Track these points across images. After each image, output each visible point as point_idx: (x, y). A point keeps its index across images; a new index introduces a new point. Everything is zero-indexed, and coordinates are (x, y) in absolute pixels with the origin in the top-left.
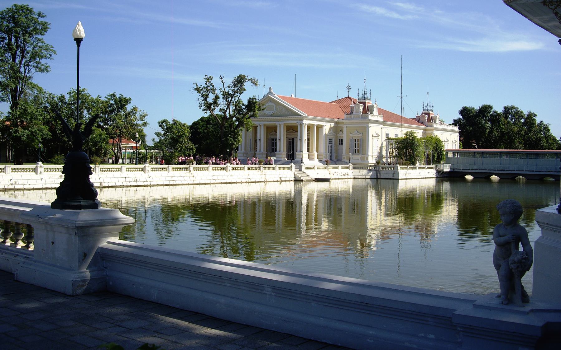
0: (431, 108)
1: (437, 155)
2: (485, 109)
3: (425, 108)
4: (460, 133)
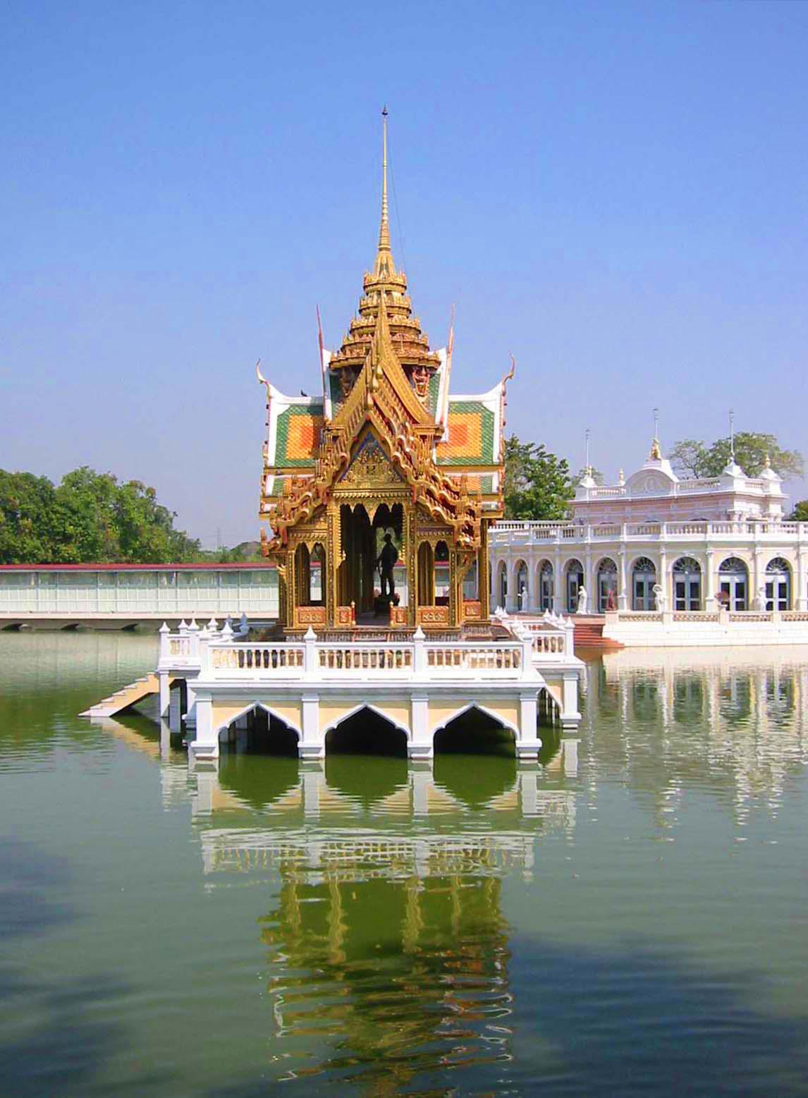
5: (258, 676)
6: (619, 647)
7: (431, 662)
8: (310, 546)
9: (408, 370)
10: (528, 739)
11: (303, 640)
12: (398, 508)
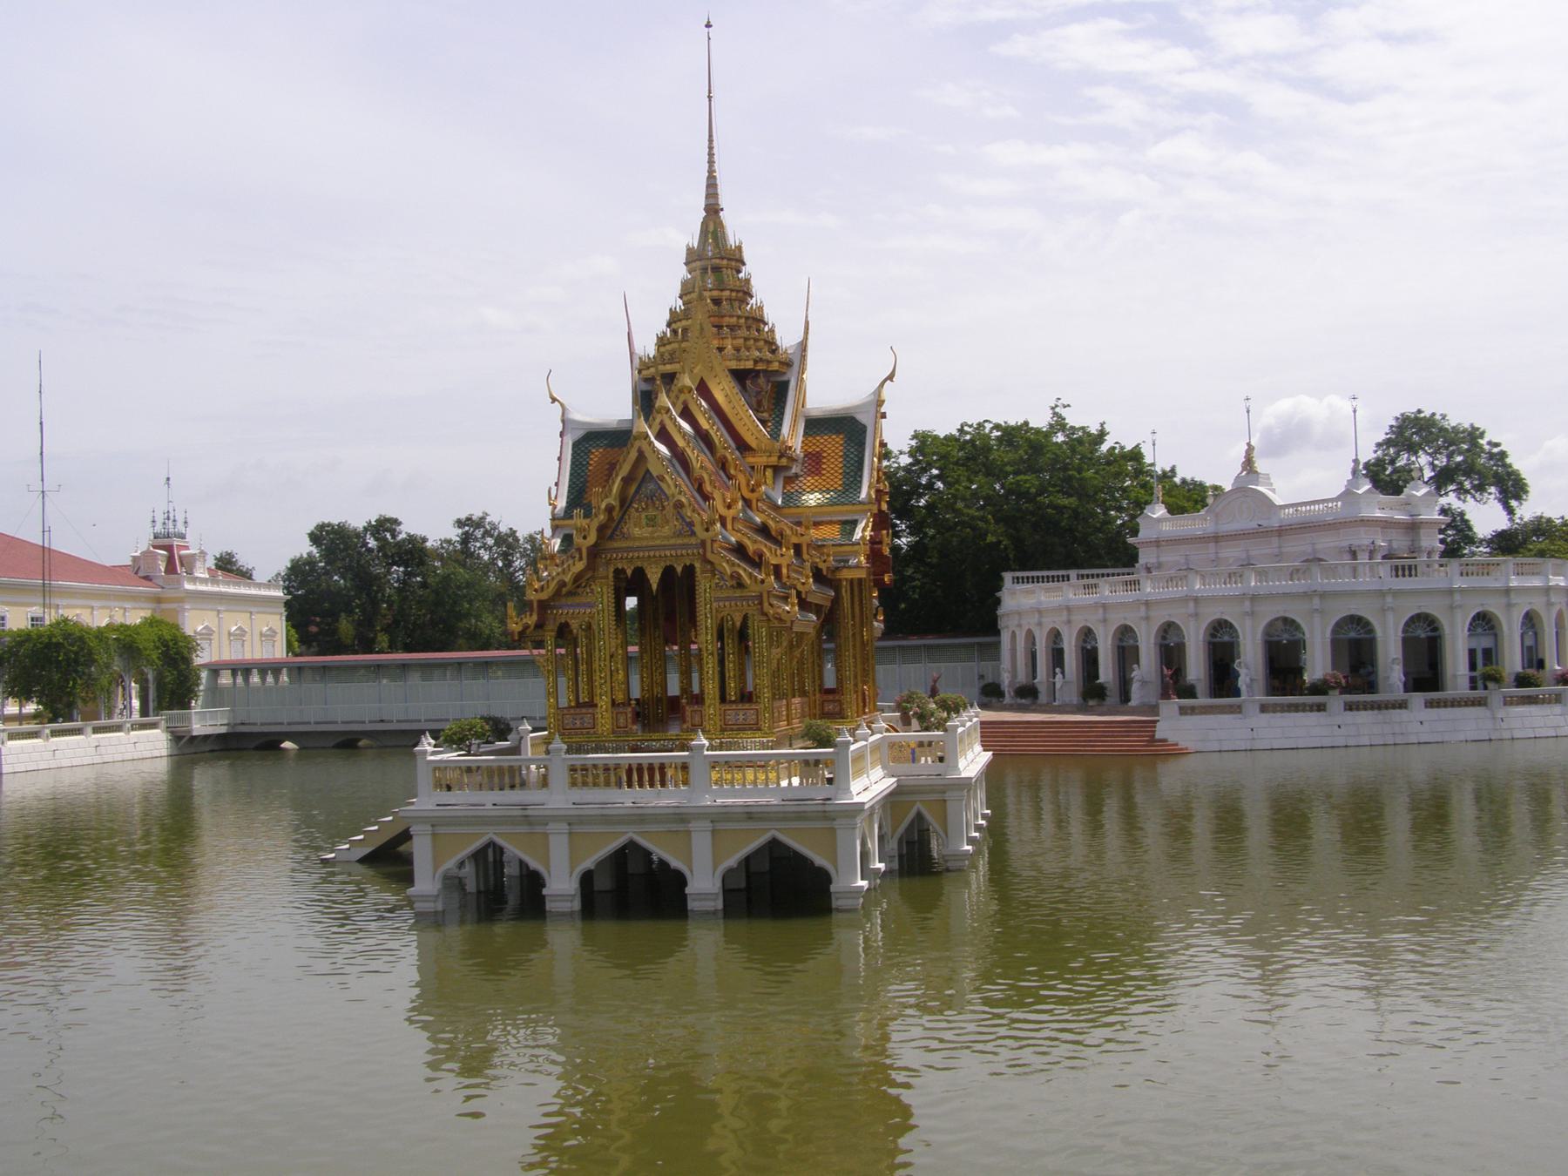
0: (181, 528)
1: (168, 671)
2: (385, 526)
3: (159, 528)
4: (287, 604)
5: (627, 798)
6: (1177, 753)
7: (574, 784)
8: (574, 625)
9: (740, 376)
10: (858, 870)
11: (688, 749)
12: (689, 570)
